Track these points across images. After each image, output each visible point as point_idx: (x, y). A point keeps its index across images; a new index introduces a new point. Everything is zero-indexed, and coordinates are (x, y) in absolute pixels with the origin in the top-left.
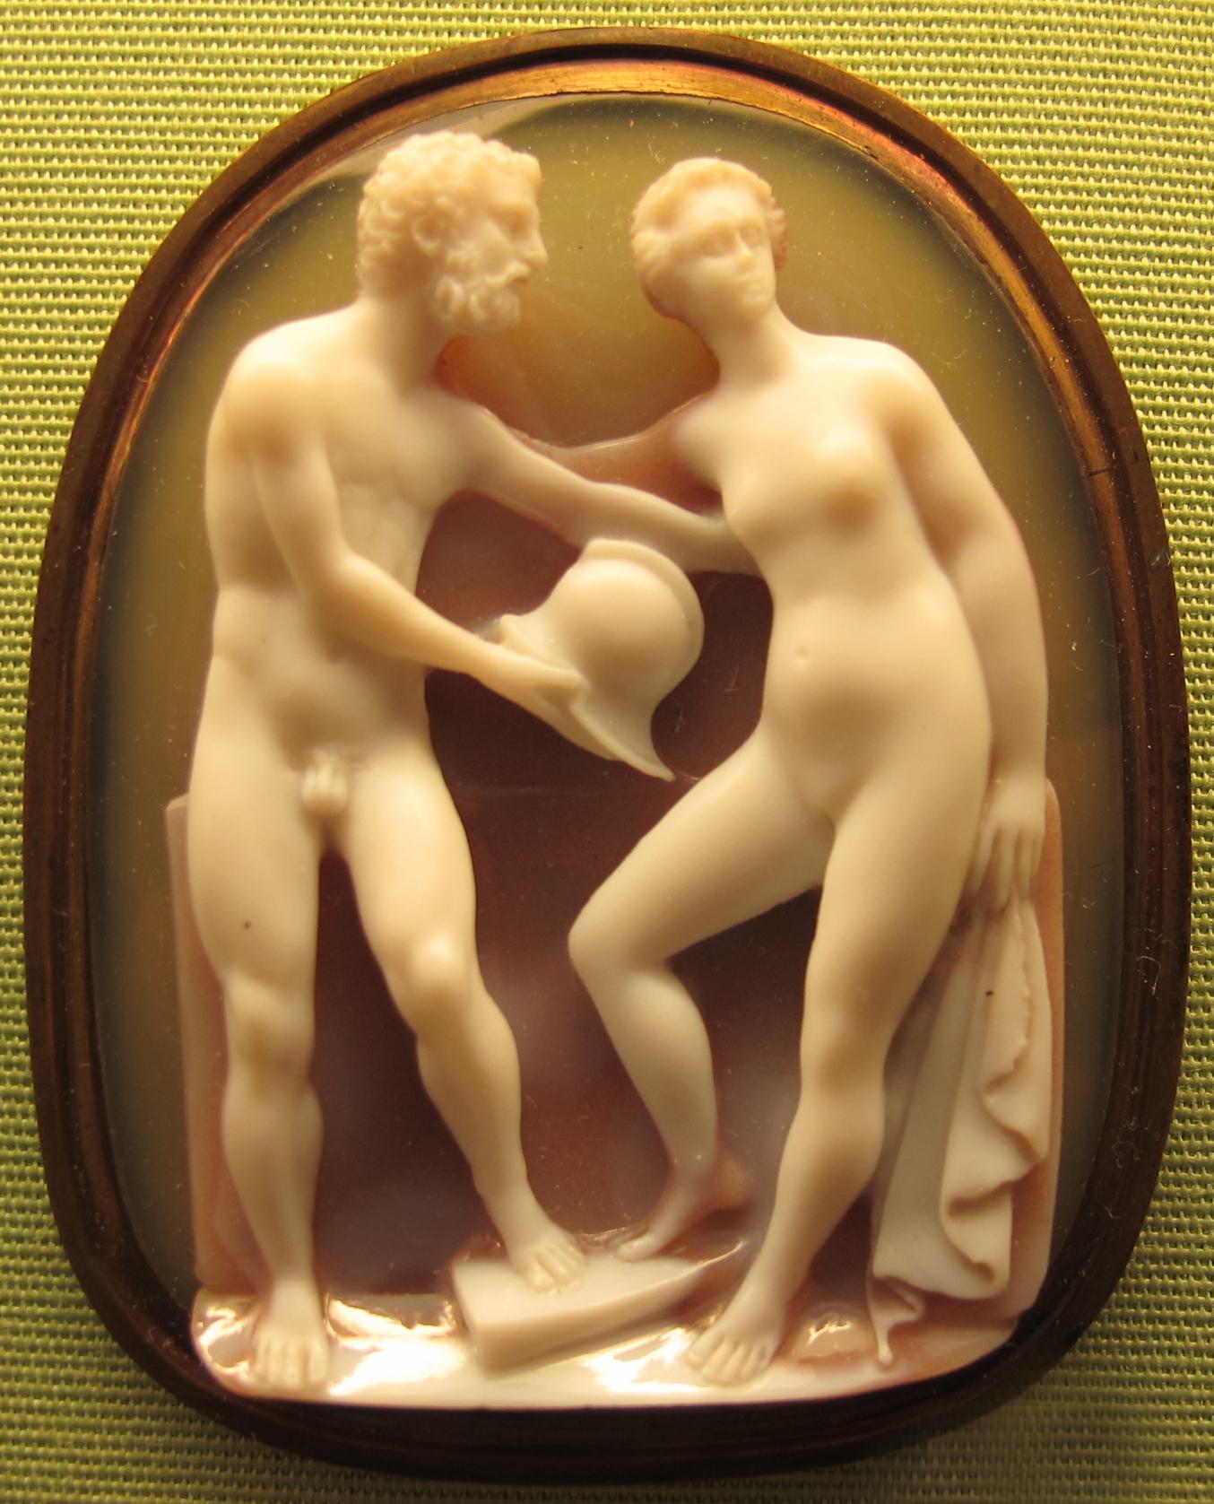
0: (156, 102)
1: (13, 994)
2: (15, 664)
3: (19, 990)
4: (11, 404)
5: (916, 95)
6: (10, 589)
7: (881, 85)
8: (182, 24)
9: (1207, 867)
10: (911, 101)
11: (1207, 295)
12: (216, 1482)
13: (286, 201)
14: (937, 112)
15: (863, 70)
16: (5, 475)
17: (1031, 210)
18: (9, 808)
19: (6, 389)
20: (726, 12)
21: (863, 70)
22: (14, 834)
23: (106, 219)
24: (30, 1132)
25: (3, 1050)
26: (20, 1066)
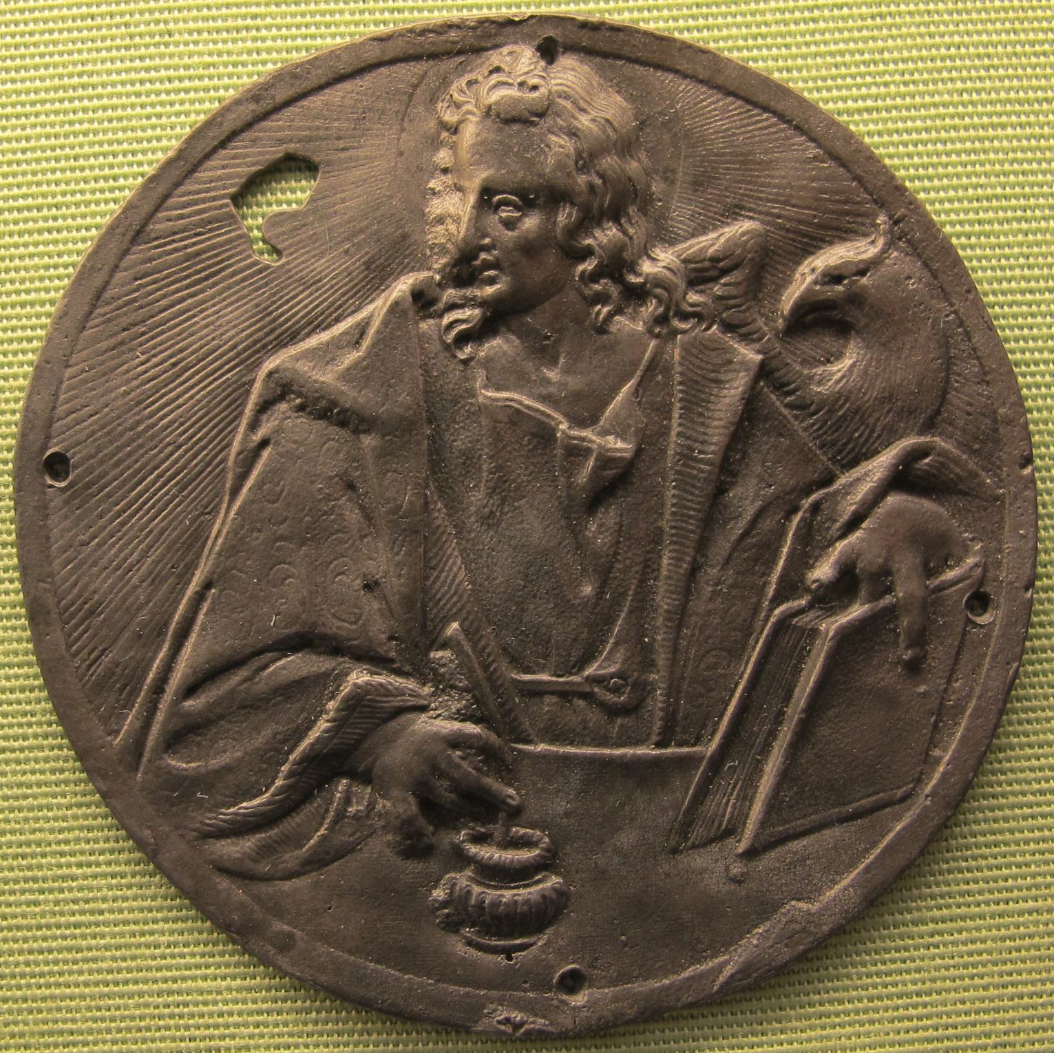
0: (242, 53)
1: (12, 597)
2: (11, 260)
3: (17, 592)
4: (9, 16)
5: (780, 70)
6: (6, 345)
7: (806, 94)
8: (100, 177)
9: (1049, 493)
10: (776, 75)
11: (1050, 260)
12: (316, 1022)
13: (874, 798)
14: (826, 101)
15: (761, 64)
16: (5, 330)
17: (876, 151)
18: (7, 562)
19: (4, 122)
20: (723, 8)
21: (761, 64)
22: (9, 556)
23: (158, 93)
24: (35, 677)
25: (1, 811)
26: (18, 617)
